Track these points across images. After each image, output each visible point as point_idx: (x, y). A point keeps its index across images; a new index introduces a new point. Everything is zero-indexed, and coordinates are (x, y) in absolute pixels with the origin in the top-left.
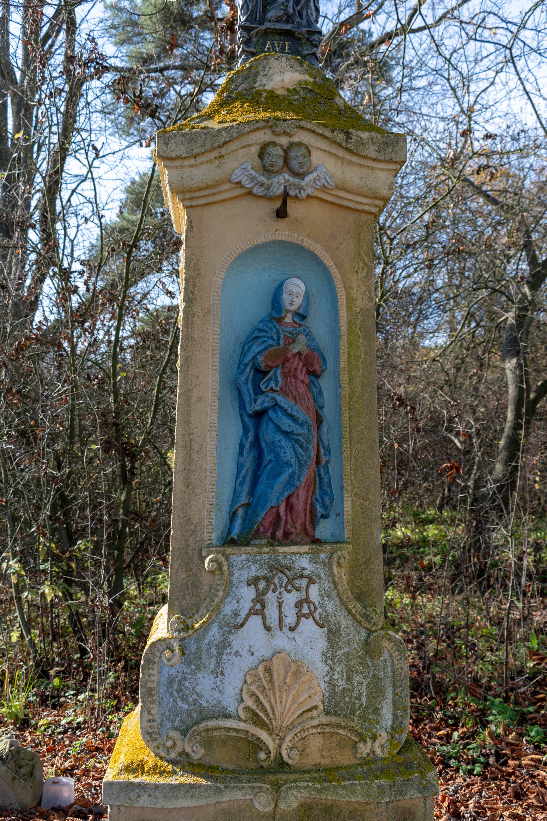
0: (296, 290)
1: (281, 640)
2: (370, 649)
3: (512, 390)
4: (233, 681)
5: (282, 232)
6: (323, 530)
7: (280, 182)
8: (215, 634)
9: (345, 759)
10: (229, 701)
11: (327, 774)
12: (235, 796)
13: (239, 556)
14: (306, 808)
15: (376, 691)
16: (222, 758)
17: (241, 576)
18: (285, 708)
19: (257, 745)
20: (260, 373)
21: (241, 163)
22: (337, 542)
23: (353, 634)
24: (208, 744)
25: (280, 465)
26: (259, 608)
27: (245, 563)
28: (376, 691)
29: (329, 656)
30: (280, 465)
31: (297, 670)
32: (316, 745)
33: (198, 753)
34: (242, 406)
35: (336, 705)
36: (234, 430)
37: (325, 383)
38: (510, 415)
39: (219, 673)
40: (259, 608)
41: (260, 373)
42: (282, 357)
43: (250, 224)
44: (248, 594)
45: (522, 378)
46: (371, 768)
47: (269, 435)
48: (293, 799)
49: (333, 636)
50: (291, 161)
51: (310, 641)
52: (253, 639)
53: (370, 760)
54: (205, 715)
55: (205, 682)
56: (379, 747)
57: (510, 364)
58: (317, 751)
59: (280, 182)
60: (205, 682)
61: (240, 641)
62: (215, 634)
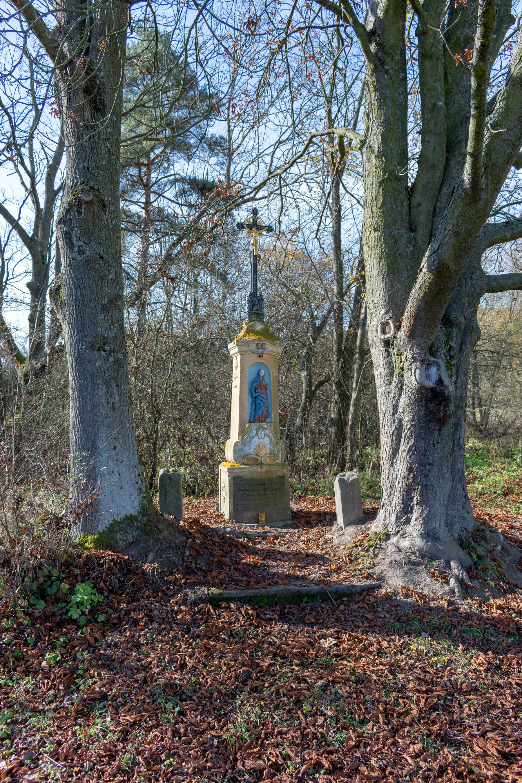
0: (263, 372)
1: (261, 440)
2: (277, 443)
3: (304, 386)
4: (252, 448)
5: (260, 360)
6: (268, 420)
7: (260, 351)
8: (249, 439)
9: (273, 463)
10: (252, 452)
11: (270, 465)
12: (254, 468)
13: (253, 425)
14: (266, 471)
15: (278, 451)
16: (250, 462)
17: (253, 428)
18: (262, 453)
19: (257, 460)
20: (256, 389)
21: (253, 347)
22: (271, 422)
23: (274, 440)
24: (248, 460)
25: (260, 407)
26: (257, 434)
27: (254, 426)
28: (278, 451)
29: (270, 443)
30: (260, 407)
31: (265, 446)
32: (268, 460)
33: (246, 462)
34: (252, 395)
35: (271, 453)
36: (250, 400)
37: (268, 391)
38: (303, 397)
39: (250, 447)
40: (257, 434)
41: (256, 389)
42: (260, 385)
43: (254, 359)
44: (255, 432)
45: (310, 382)
46: (278, 465)
47: (258, 401)
48: (264, 469)
49: (271, 440)
50: (263, 347)
51: (266, 441)
52: (256, 440)
53: (277, 464)
54: (247, 455)
55: (247, 449)
56: (279, 461)
57: (304, 374)
58: (268, 461)
59: (260, 351)
60: (247, 449)
61: (254, 440)
62: (249, 439)
